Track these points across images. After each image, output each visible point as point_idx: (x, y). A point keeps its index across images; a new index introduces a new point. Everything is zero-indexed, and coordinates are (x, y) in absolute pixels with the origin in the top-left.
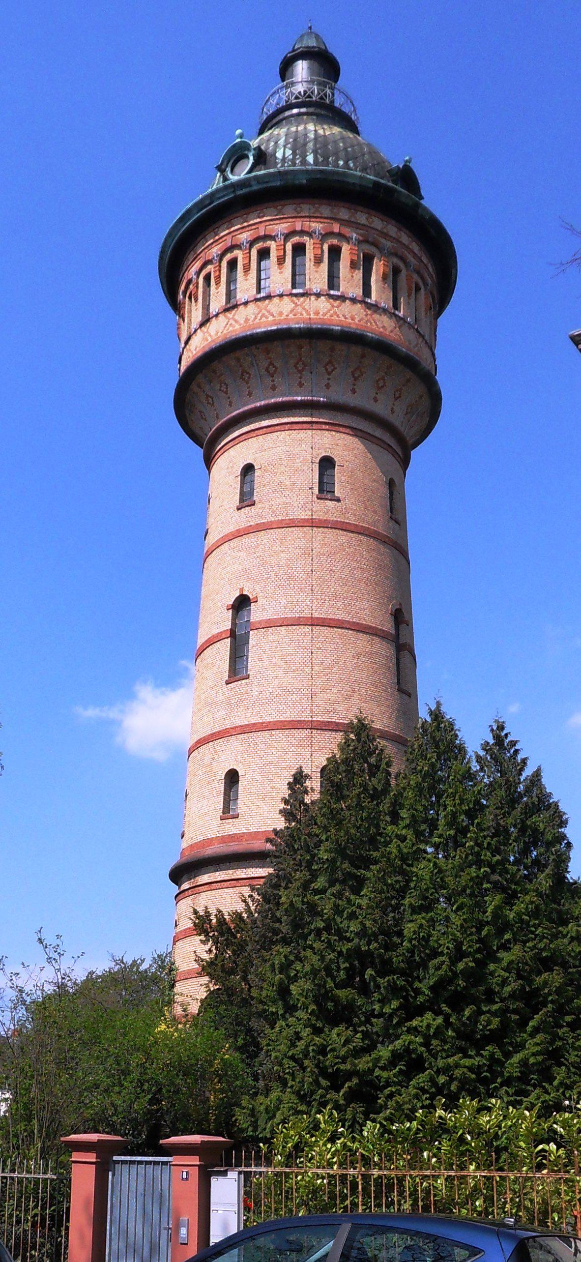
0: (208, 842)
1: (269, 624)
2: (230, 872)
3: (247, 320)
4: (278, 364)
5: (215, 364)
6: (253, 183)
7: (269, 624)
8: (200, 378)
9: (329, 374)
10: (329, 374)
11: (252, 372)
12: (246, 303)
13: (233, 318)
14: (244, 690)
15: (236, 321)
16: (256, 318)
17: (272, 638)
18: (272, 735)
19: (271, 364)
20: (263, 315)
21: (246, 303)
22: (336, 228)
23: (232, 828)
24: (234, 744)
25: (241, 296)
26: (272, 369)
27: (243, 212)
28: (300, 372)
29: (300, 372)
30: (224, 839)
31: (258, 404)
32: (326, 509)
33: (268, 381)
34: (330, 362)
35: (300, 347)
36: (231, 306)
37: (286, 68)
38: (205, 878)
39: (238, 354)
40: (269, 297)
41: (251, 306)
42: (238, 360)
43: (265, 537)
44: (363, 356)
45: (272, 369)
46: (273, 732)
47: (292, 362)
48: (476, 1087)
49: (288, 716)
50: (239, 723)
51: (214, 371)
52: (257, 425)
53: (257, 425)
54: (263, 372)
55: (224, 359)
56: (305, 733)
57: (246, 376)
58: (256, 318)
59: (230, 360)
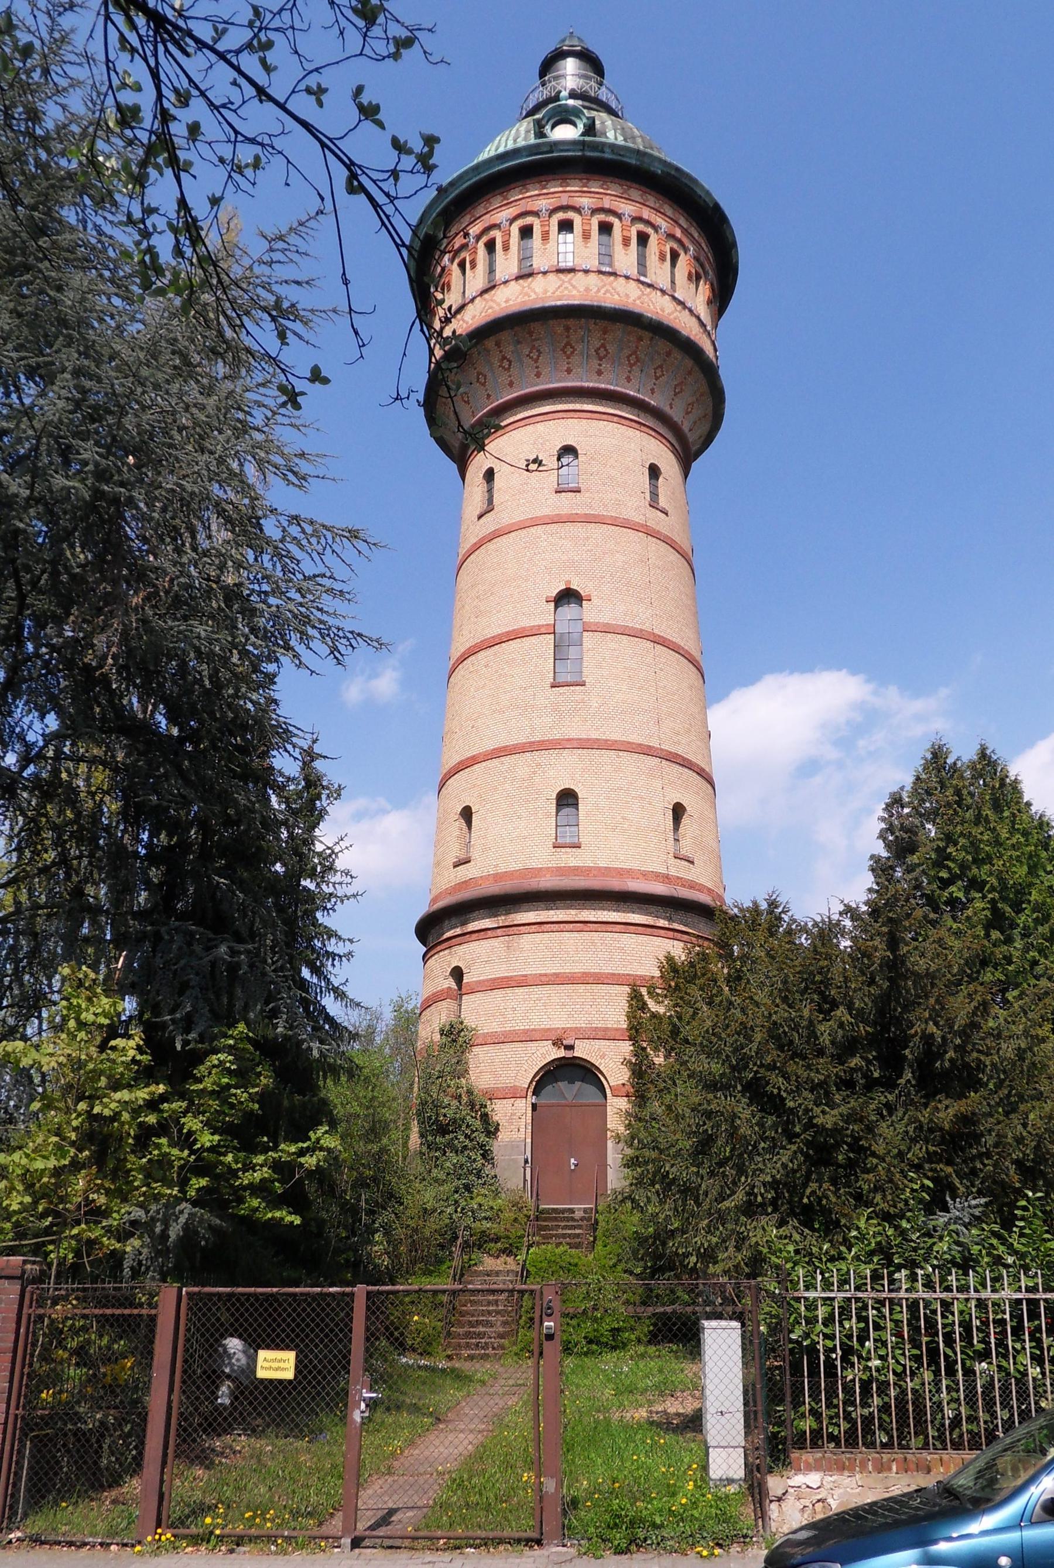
0: (538, 872)
1: (607, 630)
2: (573, 912)
3: (587, 290)
4: (611, 349)
5: (535, 326)
6: (607, 150)
7: (607, 630)
8: (505, 336)
9: (657, 378)
10: (657, 378)
11: (579, 347)
12: (505, 282)
13: (569, 282)
14: (578, 697)
15: (574, 287)
16: (599, 290)
17: (613, 645)
18: (618, 757)
19: (603, 346)
20: (607, 291)
21: (505, 282)
22: (678, 233)
23: (570, 859)
24: (570, 758)
25: (500, 275)
26: (602, 352)
27: (583, 175)
28: (631, 365)
29: (631, 365)
30: (561, 871)
31: (586, 384)
32: (654, 519)
33: (595, 362)
34: (661, 367)
35: (640, 339)
36: (525, 275)
37: (548, 65)
38: (531, 916)
39: (571, 322)
40: (614, 274)
41: (592, 276)
42: (567, 329)
43: (597, 532)
44: (690, 373)
45: (602, 352)
46: (621, 753)
47: (626, 352)
48: (141, 1125)
49: (635, 738)
50: (573, 735)
51: (531, 333)
52: (578, 406)
53: (578, 406)
54: (592, 352)
55: (551, 322)
56: (655, 761)
57: (569, 351)
58: (599, 290)
59: (558, 326)
